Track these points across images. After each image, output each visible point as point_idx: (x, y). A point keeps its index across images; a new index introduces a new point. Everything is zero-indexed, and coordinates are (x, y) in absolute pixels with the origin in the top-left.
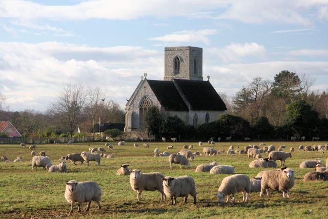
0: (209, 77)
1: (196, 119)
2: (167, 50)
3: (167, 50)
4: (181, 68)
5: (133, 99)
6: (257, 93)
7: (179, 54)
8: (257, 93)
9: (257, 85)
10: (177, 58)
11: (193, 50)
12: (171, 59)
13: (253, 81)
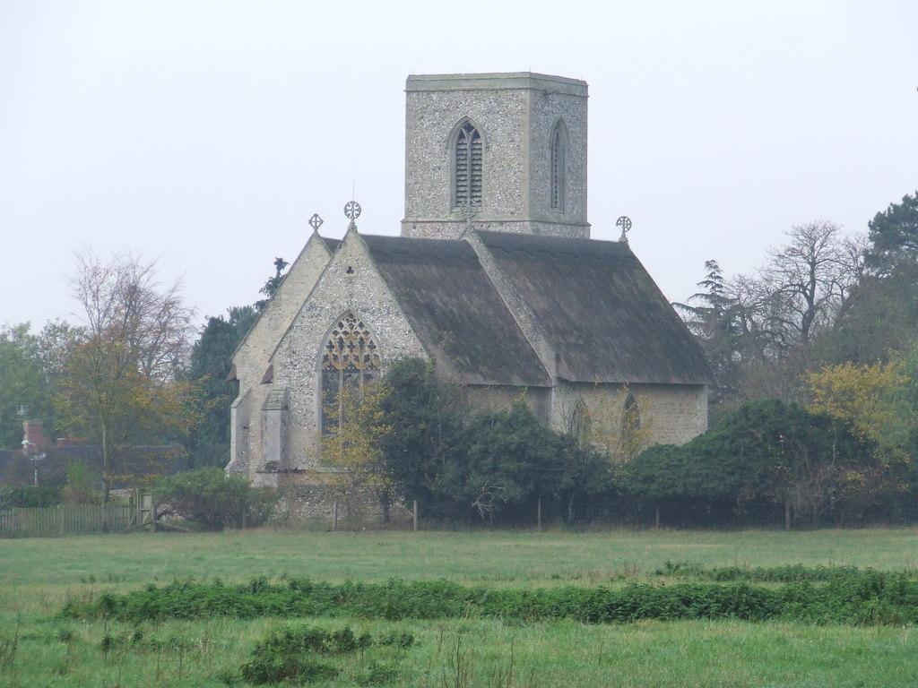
0: (625, 223)
1: (579, 417)
2: (417, 87)
3: (417, 87)
4: (489, 181)
5: (480, 386)
6: (810, 299)
7: (476, 111)
8: (810, 299)
9: (813, 264)
10: (469, 127)
11: (545, 94)
12: (438, 134)
13: (789, 242)
